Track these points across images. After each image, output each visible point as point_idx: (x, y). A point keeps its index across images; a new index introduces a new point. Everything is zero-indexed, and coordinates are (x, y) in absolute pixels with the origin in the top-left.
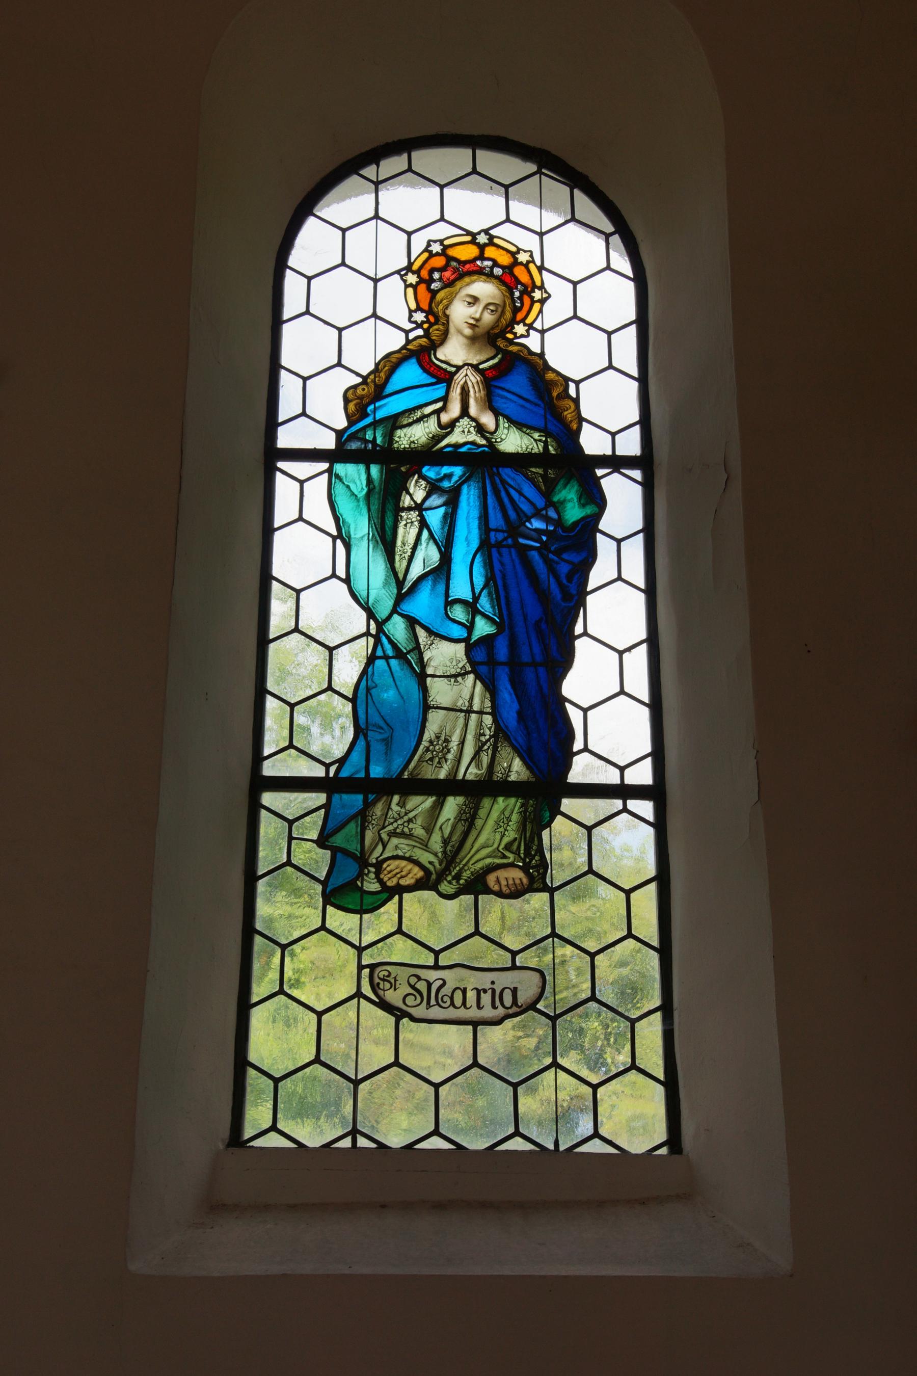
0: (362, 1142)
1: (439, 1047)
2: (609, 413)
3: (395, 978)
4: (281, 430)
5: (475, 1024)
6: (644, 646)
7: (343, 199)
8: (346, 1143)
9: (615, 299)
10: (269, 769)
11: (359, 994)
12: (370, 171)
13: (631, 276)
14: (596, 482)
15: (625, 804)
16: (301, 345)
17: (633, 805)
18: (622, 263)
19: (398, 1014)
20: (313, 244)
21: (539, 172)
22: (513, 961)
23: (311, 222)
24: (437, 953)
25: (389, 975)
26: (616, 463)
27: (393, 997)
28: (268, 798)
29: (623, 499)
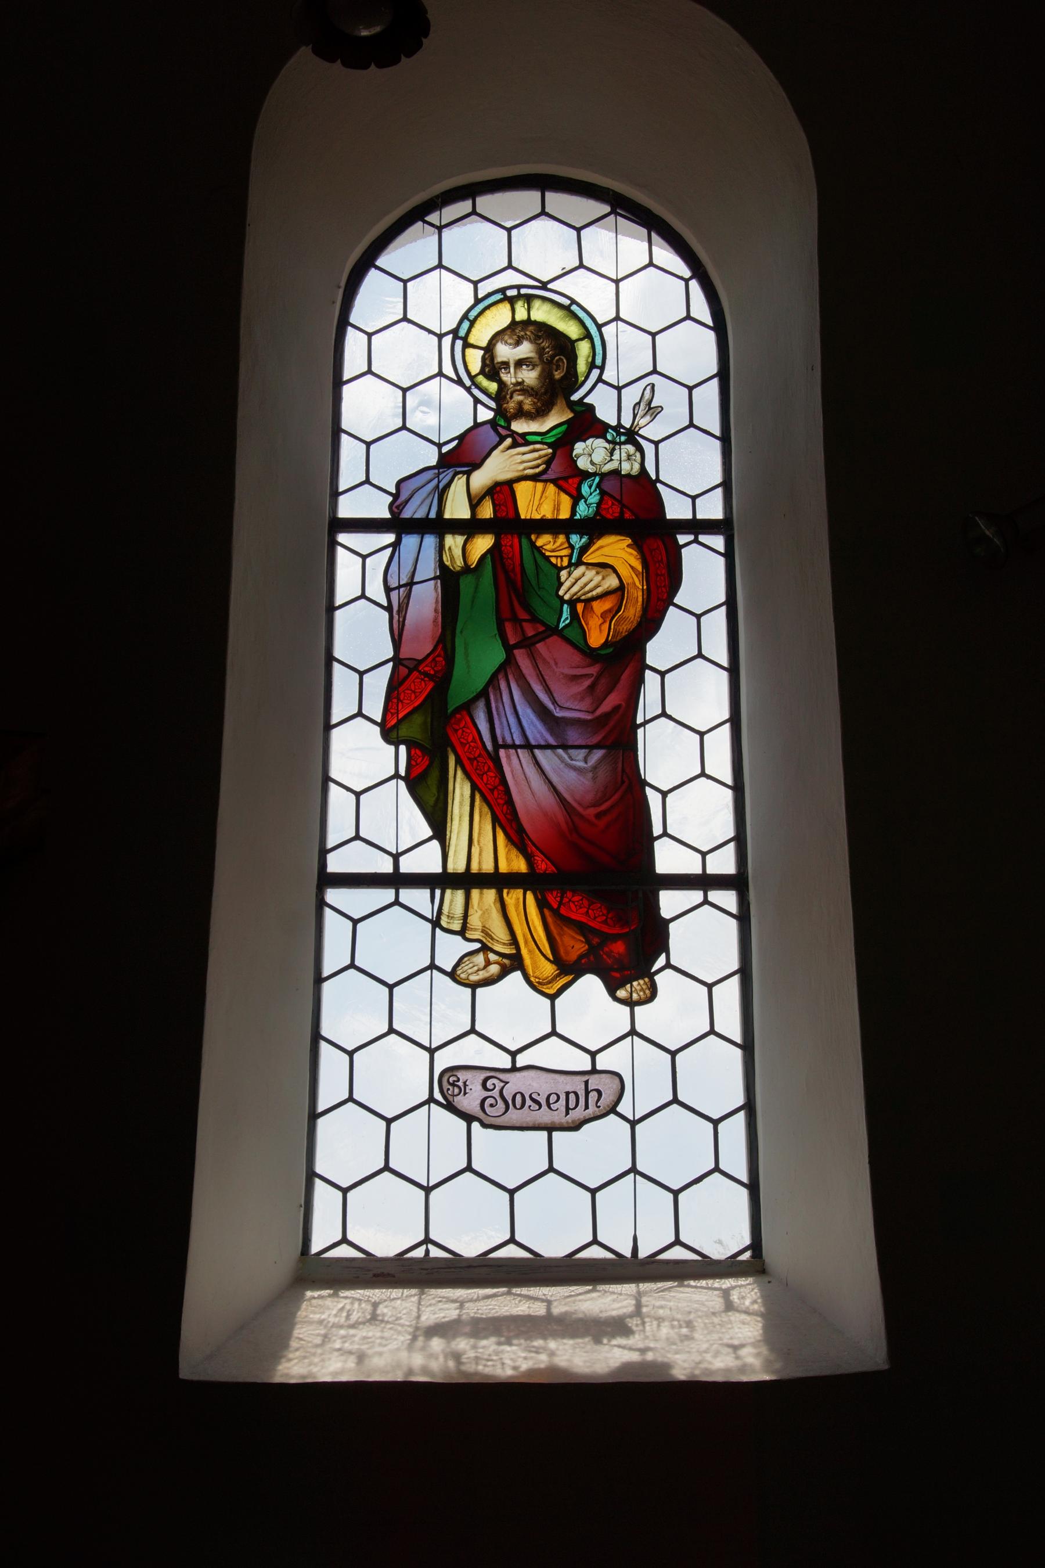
0: (435, 1252)
1: (510, 1153)
2: (690, 473)
3: (465, 1083)
4: (342, 499)
5: (550, 1129)
6: (728, 725)
7: (403, 245)
8: (419, 1253)
9: (694, 351)
10: (335, 864)
11: (431, 1100)
12: (433, 218)
13: (711, 324)
14: (675, 553)
15: (706, 896)
16: (364, 406)
17: (714, 896)
18: (701, 309)
19: (469, 1118)
20: (375, 299)
21: (613, 212)
22: (514, 1062)
23: (373, 273)
24: (514, 1054)
25: (458, 1080)
26: (697, 527)
27: (469, 1102)
28: (333, 896)
29: (703, 571)
